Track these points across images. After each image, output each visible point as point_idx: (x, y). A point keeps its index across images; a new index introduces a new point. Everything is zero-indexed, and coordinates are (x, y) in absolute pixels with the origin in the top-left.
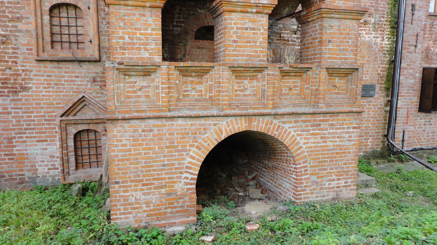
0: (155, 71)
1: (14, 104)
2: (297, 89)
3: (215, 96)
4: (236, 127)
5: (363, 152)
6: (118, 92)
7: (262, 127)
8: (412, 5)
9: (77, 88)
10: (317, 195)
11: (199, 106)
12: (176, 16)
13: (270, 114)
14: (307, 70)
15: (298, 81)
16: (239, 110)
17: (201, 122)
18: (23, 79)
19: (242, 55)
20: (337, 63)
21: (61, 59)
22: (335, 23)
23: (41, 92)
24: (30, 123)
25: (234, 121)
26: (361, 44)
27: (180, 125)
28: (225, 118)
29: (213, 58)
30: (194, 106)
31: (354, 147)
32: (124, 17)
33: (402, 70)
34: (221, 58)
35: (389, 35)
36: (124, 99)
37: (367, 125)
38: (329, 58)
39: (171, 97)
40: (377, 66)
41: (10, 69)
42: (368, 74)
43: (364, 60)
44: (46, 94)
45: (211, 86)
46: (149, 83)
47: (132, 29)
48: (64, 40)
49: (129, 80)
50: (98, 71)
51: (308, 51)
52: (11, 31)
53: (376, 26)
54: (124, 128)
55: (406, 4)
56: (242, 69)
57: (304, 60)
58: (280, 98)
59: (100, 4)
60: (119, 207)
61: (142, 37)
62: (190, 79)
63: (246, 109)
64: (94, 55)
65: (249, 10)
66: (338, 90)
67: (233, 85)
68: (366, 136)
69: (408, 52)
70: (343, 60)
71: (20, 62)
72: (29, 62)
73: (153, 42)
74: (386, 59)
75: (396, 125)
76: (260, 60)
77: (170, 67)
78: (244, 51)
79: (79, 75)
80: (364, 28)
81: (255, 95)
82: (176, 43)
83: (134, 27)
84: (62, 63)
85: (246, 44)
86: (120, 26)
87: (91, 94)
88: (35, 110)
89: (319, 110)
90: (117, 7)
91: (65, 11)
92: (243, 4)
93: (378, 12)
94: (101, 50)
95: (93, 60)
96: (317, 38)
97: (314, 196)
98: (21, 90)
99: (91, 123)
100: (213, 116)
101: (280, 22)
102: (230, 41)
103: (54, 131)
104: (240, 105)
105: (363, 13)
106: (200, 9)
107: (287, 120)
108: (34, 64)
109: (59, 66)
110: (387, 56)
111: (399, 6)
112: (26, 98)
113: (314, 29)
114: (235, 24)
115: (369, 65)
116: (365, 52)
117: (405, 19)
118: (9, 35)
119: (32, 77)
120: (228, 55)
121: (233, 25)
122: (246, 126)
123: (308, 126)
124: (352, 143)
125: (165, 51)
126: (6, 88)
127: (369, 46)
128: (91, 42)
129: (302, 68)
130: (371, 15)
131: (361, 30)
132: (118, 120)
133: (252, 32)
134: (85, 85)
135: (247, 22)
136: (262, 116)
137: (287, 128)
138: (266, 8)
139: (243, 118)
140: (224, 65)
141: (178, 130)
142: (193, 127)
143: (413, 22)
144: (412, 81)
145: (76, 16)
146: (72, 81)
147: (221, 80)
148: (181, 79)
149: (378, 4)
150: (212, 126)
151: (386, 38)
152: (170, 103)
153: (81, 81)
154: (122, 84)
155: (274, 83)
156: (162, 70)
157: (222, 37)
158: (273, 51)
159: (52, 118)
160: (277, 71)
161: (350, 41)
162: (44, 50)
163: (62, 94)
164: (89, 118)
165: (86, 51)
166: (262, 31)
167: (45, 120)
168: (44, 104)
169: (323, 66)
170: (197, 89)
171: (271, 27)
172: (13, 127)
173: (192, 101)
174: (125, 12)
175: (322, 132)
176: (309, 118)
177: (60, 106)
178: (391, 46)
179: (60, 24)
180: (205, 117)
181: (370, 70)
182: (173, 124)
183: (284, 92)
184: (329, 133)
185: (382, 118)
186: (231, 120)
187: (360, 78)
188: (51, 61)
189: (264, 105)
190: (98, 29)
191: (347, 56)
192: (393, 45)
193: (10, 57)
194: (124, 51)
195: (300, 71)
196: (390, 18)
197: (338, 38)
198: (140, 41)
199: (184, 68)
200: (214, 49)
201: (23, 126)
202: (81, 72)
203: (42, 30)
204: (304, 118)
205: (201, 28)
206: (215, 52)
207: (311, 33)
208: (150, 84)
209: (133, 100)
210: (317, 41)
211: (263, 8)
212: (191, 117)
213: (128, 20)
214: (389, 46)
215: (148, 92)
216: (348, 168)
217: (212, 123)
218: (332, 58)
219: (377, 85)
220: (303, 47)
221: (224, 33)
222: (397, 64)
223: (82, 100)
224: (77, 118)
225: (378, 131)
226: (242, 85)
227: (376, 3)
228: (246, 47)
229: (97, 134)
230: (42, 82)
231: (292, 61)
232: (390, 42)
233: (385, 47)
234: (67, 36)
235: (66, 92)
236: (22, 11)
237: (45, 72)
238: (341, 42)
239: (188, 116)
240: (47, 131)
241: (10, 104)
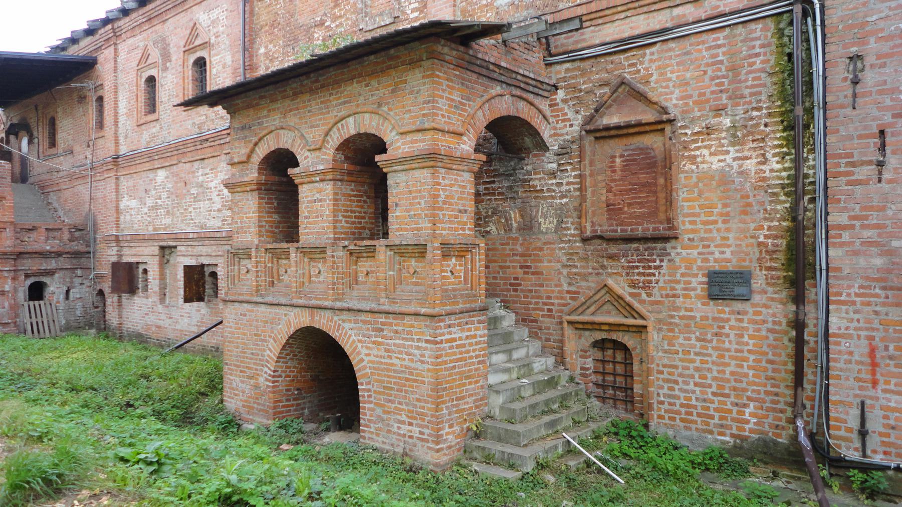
5: (732, 435)
10: (385, 440)
19: (312, 233)
31: (430, 374)
35: (781, 146)
38: (398, 230)
40: (752, 226)
42: (729, 246)
53: (739, 134)
55: (824, 62)
60: (573, 227)
63: (310, 299)
65: (313, 179)
68: (736, 396)
93: (742, 101)
97: (380, 439)
110: (783, 198)
115: (727, 226)
123: (368, 329)
124: (426, 366)
127: (724, 180)
131: (698, 148)
144: (878, 262)
149: (740, 82)
151: (774, 155)
161: (422, 201)
176: (369, 317)
181: (731, 236)
184: (395, 345)
185: (784, 358)
196: (780, 107)
204: (363, 317)
214: (784, 174)
216: (423, 408)
218: (402, 230)
228: (315, 223)
231: (552, 227)
232: (787, 165)
238: (411, 204)
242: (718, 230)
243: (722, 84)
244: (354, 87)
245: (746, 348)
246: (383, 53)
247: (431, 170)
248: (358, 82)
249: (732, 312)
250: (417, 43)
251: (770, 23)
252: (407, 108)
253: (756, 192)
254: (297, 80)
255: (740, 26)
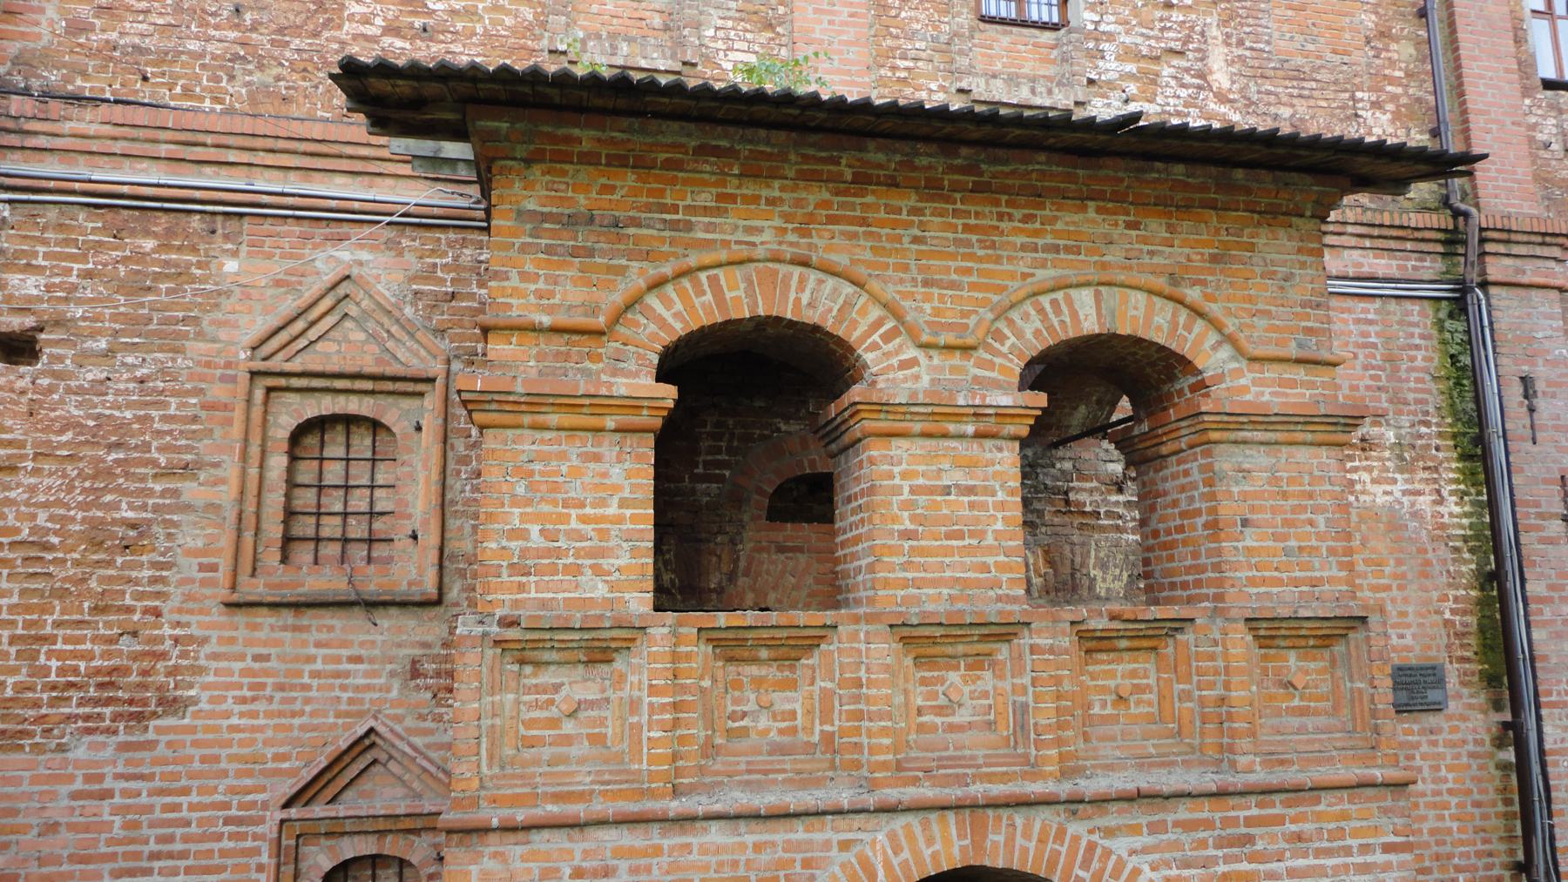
0: (627, 645)
1: (128, 763)
2: (1146, 697)
3: (843, 732)
4: (927, 852)
6: (493, 726)
7: (1025, 851)
8: (1522, 378)
9: (351, 701)
11: (784, 771)
12: (705, 444)
13: (1051, 799)
14: (1176, 629)
15: (1146, 665)
16: (934, 785)
17: (792, 836)
18: (173, 672)
19: (935, 583)
20: (1283, 599)
21: (310, 600)
22: (1257, 459)
23: (227, 715)
24: (171, 830)
25: (917, 830)
26: (1361, 519)
27: (713, 848)
28: (884, 817)
29: (833, 592)
30: (766, 772)
32: (532, 466)
33: (1533, 607)
34: (863, 594)
36: (511, 752)
37: (1440, 824)
38: (1252, 582)
39: (682, 740)
40: (1435, 595)
41: (135, 634)
42: (1409, 626)
43: (1381, 574)
44: (243, 721)
45: (827, 695)
46: (603, 691)
47: (556, 505)
48: (355, 468)
49: (534, 681)
50: (429, 638)
51: (1171, 558)
52: (157, 509)
53: (1406, 455)
54: (505, 861)
55: (1498, 376)
56: (938, 632)
57: (1162, 588)
58: (1085, 733)
59: (454, 415)
61: (588, 529)
62: (754, 670)
63: (961, 780)
64: (420, 583)
65: (952, 428)
66: (1301, 699)
67: (906, 692)
68: (1443, 869)
69: (1542, 541)
70: (1304, 589)
71: (171, 612)
72: (201, 612)
73: (625, 545)
74: (1464, 569)
75: (1556, 820)
76: (999, 599)
77: (682, 630)
78: (942, 567)
79: (363, 652)
80: (1365, 463)
81: (989, 725)
82: (704, 535)
83: (560, 496)
84: (310, 612)
85: (945, 543)
86: (514, 496)
87: (399, 719)
88: (196, 783)
89: (1238, 781)
90: (510, 432)
91: (341, 439)
92: (930, 409)
93: (1406, 408)
94: (446, 563)
95: (417, 598)
96: (1198, 512)
98: (160, 709)
99: (390, 831)
100: (839, 812)
101: (1061, 452)
102: (891, 532)
103: (253, 861)
104: (939, 767)
105: (1352, 421)
106: (787, 418)
107: (1121, 821)
108: (217, 615)
109: (298, 622)
110: (1467, 556)
111: (1475, 383)
112: (171, 737)
113: (1183, 481)
114: (905, 475)
115: (1406, 593)
116: (1381, 546)
117: (1508, 426)
118: (149, 522)
119: (202, 662)
120: (887, 584)
121: (897, 481)
122: (963, 849)
123: (1203, 844)
125: (666, 563)
126: (108, 702)
127: (1394, 524)
128: (414, 537)
129: (1156, 620)
130: (1379, 417)
131: (1355, 470)
132: (484, 830)
133: (966, 499)
134: (381, 690)
135: (947, 466)
136: (1024, 810)
137: (1125, 855)
138: (1008, 420)
139: (951, 816)
140: (871, 618)
141: (706, 868)
142: (765, 857)
143: (1539, 435)
145: (374, 452)
146: (337, 675)
147: (863, 674)
148: (720, 674)
149: (1400, 380)
150: (834, 852)
151: (1452, 493)
152: (680, 763)
153: (367, 674)
154: (511, 696)
155: (1058, 681)
156: (652, 641)
157: (862, 521)
158: (1046, 552)
159: (252, 812)
160: (1064, 633)
161: (1320, 520)
162: (254, 569)
163: (297, 721)
164: (382, 812)
165: (395, 568)
166: (1001, 496)
167: (227, 821)
168: (231, 758)
169: (1234, 613)
170: (777, 707)
171: (1029, 470)
172: (110, 850)
173: (760, 753)
174: (534, 447)
175: (1261, 867)
176: (1205, 811)
177: (286, 765)
178: (1474, 520)
179: (320, 480)
180: (807, 814)
181: (1410, 609)
182: (688, 846)
183: (1096, 710)
185: (1492, 795)
186: (908, 827)
187: (1381, 653)
188: (274, 606)
189: (1028, 763)
190: (443, 495)
191: (1317, 574)
192: (1482, 516)
193: (140, 596)
194: (524, 579)
195: (1151, 632)
196: (1450, 425)
197: (1274, 510)
198: (578, 544)
199: (730, 635)
200: (837, 561)
201: (147, 842)
202: (373, 642)
203: (259, 504)
204: (1183, 812)
205: (787, 481)
206: (838, 568)
207: (1175, 496)
208: (609, 693)
209: (547, 752)
210: (1200, 521)
211: (1000, 420)
212: (756, 816)
213: (542, 473)
215: (602, 722)
217: (836, 838)
218: (1264, 581)
219: (1448, 665)
220: (1151, 542)
221: (869, 507)
222: (1512, 583)
223: (366, 743)
224: (340, 810)
225: (1487, 847)
226: (940, 689)
227: (1389, 379)
228: (948, 551)
229: (407, 872)
230: (236, 679)
231: (1119, 586)
232: (1467, 508)
233: (1454, 526)
234: (338, 520)
235: (313, 714)
236: (203, 445)
237: (249, 643)
238: (1287, 523)
239: (744, 811)
240: (229, 862)
241: (114, 762)
242: (1393, 601)
243: (1378, 378)
244: (1090, 221)
245: (1445, 787)
246: (1213, 170)
247: (1334, 452)
248: (1099, 211)
249: (1422, 732)
250: (1308, 179)
251: (1428, 307)
252: (1260, 306)
253: (1436, 545)
254: (906, 147)
255: (1393, 301)
